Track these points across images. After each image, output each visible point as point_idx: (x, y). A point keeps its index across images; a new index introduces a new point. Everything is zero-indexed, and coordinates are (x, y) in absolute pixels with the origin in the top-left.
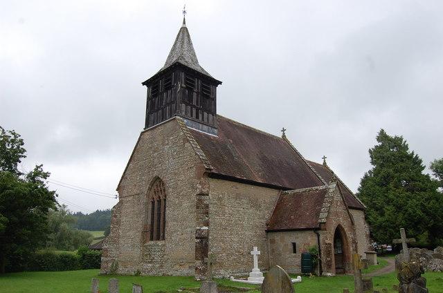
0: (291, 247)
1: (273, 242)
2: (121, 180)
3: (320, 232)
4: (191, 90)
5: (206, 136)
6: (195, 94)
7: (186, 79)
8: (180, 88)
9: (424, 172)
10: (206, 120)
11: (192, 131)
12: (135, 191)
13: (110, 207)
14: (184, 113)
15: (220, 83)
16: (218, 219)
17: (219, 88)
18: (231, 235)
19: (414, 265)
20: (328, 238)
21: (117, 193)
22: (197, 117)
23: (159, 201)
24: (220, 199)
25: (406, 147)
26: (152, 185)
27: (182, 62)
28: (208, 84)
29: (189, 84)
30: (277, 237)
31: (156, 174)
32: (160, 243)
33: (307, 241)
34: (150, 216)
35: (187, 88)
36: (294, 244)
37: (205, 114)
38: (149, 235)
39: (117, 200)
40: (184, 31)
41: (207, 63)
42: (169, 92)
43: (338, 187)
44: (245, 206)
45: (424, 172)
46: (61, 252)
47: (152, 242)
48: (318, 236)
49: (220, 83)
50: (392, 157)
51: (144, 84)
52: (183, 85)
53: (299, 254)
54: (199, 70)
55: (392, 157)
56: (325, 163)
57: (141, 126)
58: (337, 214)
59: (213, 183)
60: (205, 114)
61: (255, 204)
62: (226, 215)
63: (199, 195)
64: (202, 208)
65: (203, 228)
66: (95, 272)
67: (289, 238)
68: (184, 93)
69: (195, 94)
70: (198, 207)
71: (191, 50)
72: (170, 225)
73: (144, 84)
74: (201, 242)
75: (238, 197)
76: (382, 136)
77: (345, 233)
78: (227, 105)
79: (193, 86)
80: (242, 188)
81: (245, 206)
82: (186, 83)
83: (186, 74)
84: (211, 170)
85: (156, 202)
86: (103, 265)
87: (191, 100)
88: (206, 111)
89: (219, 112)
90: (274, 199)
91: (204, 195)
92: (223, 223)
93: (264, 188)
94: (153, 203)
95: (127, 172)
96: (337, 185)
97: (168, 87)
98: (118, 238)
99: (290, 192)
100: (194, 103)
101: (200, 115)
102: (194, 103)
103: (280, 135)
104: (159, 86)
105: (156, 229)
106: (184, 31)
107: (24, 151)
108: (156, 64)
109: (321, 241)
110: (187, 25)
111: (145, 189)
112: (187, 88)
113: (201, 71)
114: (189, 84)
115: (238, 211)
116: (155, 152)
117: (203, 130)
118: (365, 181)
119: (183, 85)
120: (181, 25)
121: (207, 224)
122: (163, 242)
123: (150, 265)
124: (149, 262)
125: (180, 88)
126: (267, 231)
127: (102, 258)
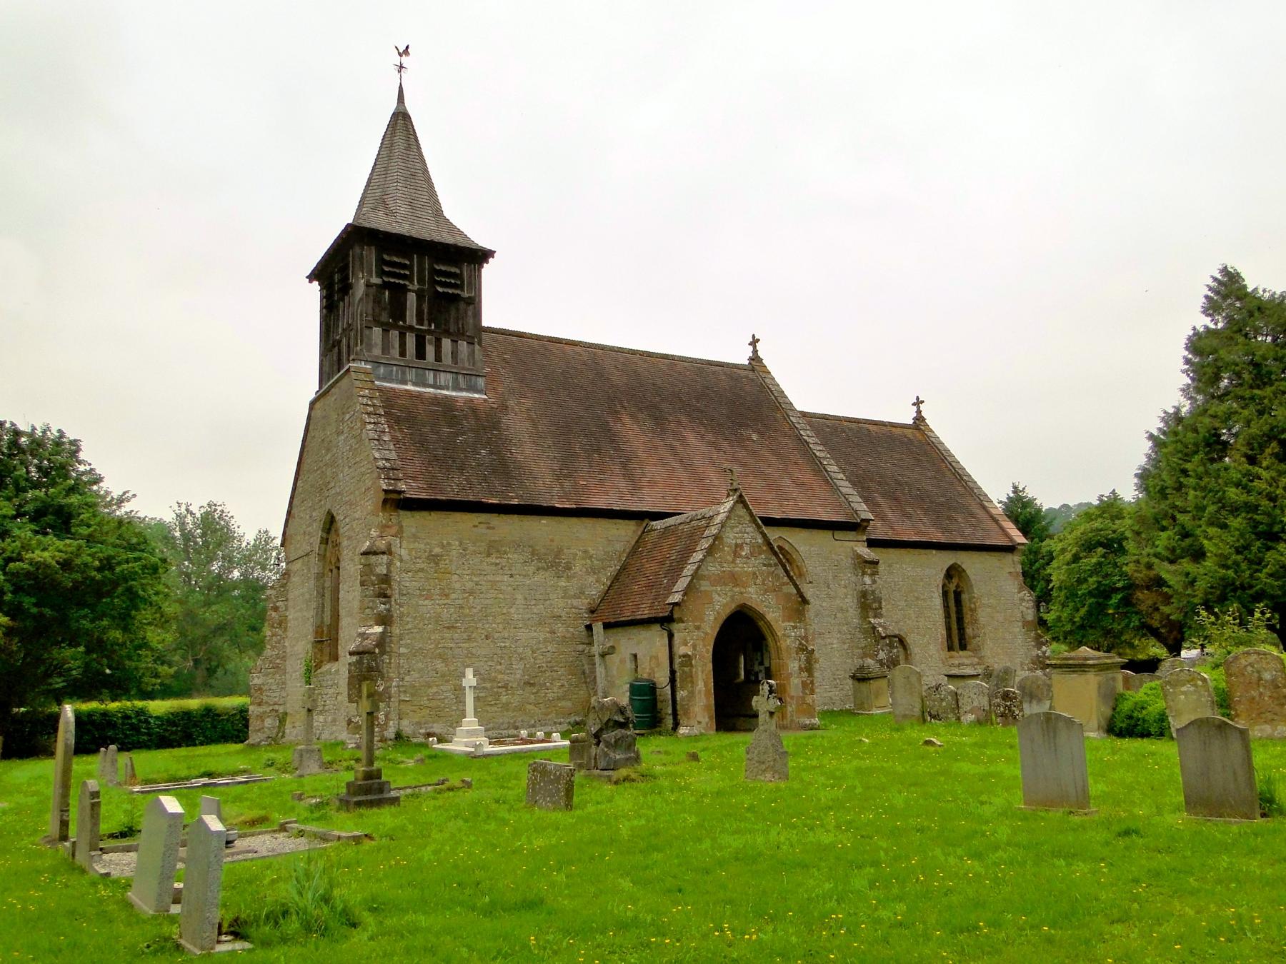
4: (399, 293)
6: (412, 298)
8: (397, 279)
10: (447, 359)
11: (380, 390)
14: (377, 351)
17: (489, 272)
18: (469, 639)
20: (697, 640)
22: (421, 354)
24: (434, 559)
26: (1089, 547)
28: (456, 263)
36: (635, 656)
37: (446, 343)
40: (401, 121)
41: (465, 212)
48: (671, 636)
57: (311, 386)
59: (411, 521)
60: (463, 345)
61: (555, 563)
65: (371, 631)
66: (239, 746)
68: (377, 301)
69: (412, 298)
74: (359, 662)
75: (493, 548)
78: (504, 303)
82: (381, 273)
83: (381, 250)
84: (400, 492)
87: (398, 311)
88: (447, 333)
89: (490, 319)
91: (375, 553)
92: (445, 615)
93: (574, 520)
95: (295, 502)
100: (411, 318)
101: (430, 350)
102: (411, 318)
103: (741, 357)
106: (401, 121)
107: (1163, 420)
115: (494, 583)
119: (375, 280)
120: (392, 106)
123: (321, 718)
125: (397, 279)
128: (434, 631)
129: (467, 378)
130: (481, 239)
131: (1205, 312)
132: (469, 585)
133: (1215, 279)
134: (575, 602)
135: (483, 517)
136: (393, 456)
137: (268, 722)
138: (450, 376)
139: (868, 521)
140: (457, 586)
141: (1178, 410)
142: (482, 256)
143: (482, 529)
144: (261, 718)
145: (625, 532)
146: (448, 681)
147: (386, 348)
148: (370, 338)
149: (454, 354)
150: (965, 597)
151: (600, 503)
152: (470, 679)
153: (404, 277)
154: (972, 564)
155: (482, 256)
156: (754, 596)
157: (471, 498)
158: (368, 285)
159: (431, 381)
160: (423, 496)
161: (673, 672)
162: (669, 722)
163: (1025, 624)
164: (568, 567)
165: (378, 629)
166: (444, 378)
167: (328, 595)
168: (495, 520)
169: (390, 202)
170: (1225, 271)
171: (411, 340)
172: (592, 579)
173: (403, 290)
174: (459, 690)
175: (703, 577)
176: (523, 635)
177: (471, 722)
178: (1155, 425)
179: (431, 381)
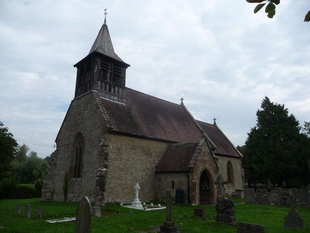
0: (171, 184)
1: (159, 180)
2: (58, 135)
3: (190, 174)
4: (105, 72)
5: (117, 104)
7: (102, 63)
8: (100, 69)
9: (301, 132)
10: (116, 93)
11: (102, 100)
12: (67, 143)
13: (49, 155)
14: (99, 88)
15: (129, 66)
16: (116, 163)
17: (128, 70)
18: (127, 174)
19: (225, 200)
20: (196, 178)
21: (55, 144)
22: (110, 90)
23: (81, 150)
24: (119, 149)
25: (286, 112)
26: (76, 138)
27: (100, 51)
29: (104, 67)
30: (162, 177)
31: (79, 131)
32: (79, 180)
33: (180, 180)
34: (75, 160)
35: (103, 70)
36: (173, 182)
37: (117, 88)
38: (73, 174)
39: (55, 149)
40: (105, 27)
42: (90, 72)
43: (206, 141)
44: (139, 154)
45: (301, 132)
46: (23, 185)
47: (74, 179)
48: (188, 177)
49: (129, 66)
50: (273, 118)
51: (75, 66)
52: (100, 68)
53: (175, 189)
54: (113, 56)
55: (273, 118)
56: (215, 123)
57: (72, 96)
58: (203, 161)
59: (113, 138)
61: (148, 153)
62: (123, 161)
63: (102, 146)
64: (104, 156)
67: (170, 178)
70: (100, 155)
71: (109, 42)
72: (86, 167)
73: (75, 66)
74: (100, 179)
76: (267, 103)
77: (211, 176)
78: (134, 81)
79: (108, 68)
80: (137, 142)
81: (139, 154)
82: (102, 66)
85: (79, 151)
86: (43, 195)
87: (105, 77)
89: (127, 85)
90: (163, 150)
94: (77, 151)
96: (206, 140)
97: (90, 69)
98: (54, 175)
99: (175, 145)
100: (108, 80)
101: (112, 90)
102: (108, 80)
103: (179, 103)
104: (84, 67)
105: (77, 170)
106: (105, 27)
108: (83, 52)
109: (190, 180)
110: (107, 24)
111: (72, 141)
112: (103, 70)
113: (117, 59)
114: (104, 67)
115: (133, 158)
116: (79, 115)
117: (115, 100)
118: (254, 135)
119: (100, 68)
121: (106, 167)
122: (80, 178)
123: (72, 195)
124: (72, 193)
125: (100, 69)
126: (156, 173)
127: (42, 190)
128: (118, 171)
129: (121, 98)
130: (126, 62)
131: (262, 107)
132: (127, 158)
133: (264, 100)
134: (153, 165)
135: (132, 138)
136: (108, 118)
137: (48, 194)
138: (117, 98)
139: (216, 148)
140: (124, 158)
141: (255, 128)
142: (127, 66)
143: (131, 142)
144: (46, 193)
145: (164, 146)
146: (121, 186)
147: (101, 87)
148: (97, 84)
149: (118, 91)
150: (231, 169)
151: (158, 137)
152: (138, 186)
153: (107, 68)
154: (233, 161)
155: (127, 66)
156: (208, 166)
157: (129, 132)
158: (98, 69)
159: (112, 98)
160: (117, 130)
161: (189, 187)
162: (187, 202)
163: (242, 177)
164: (151, 155)
165: (105, 169)
166: (116, 98)
167: (75, 158)
168: (134, 139)
169: (103, 47)
170: (266, 98)
171: (108, 86)
172: (157, 158)
173: (107, 72)
174: (133, 190)
175: (197, 161)
176: (140, 173)
177: (138, 201)
178: (249, 131)
179: (112, 98)
